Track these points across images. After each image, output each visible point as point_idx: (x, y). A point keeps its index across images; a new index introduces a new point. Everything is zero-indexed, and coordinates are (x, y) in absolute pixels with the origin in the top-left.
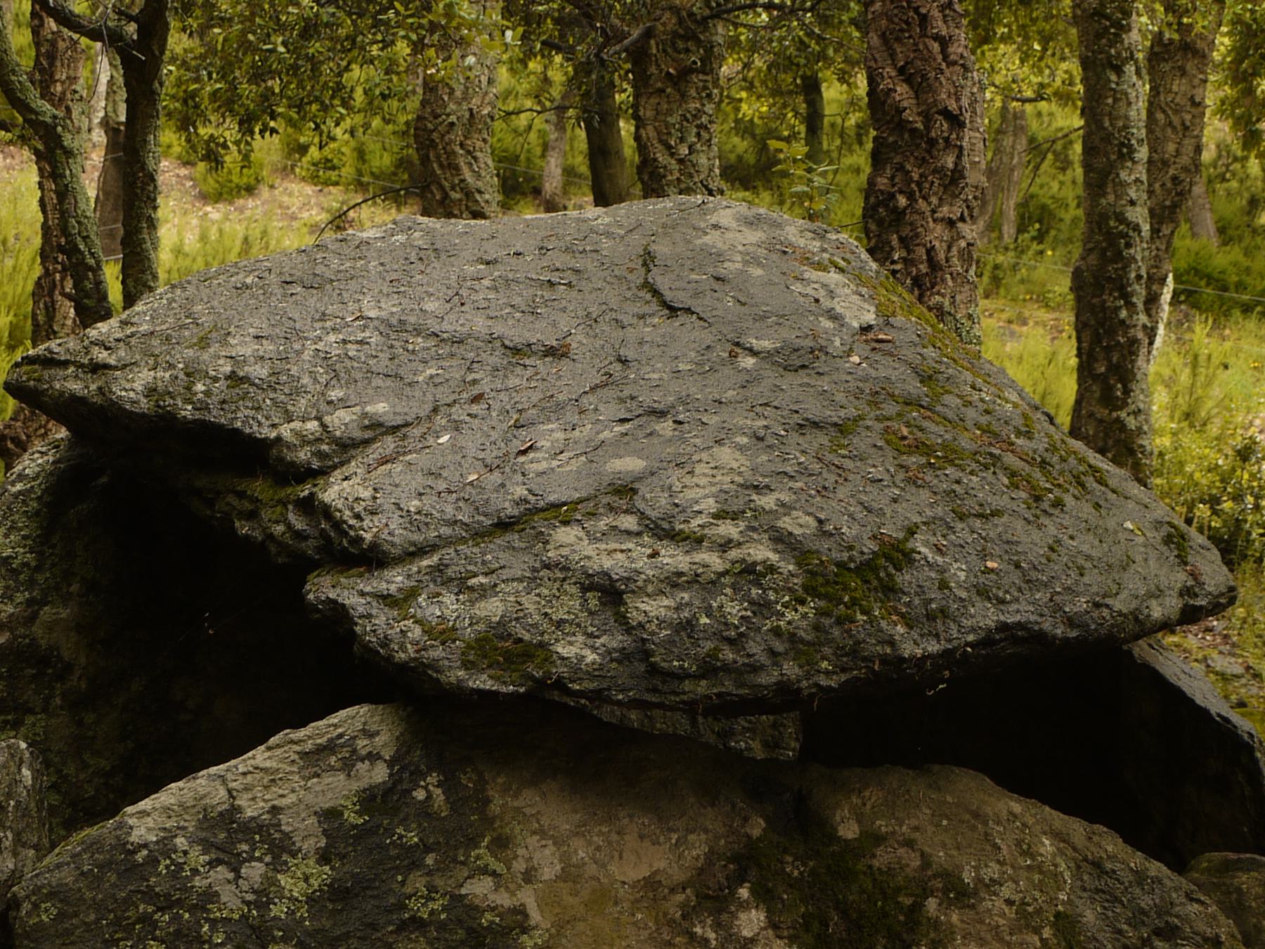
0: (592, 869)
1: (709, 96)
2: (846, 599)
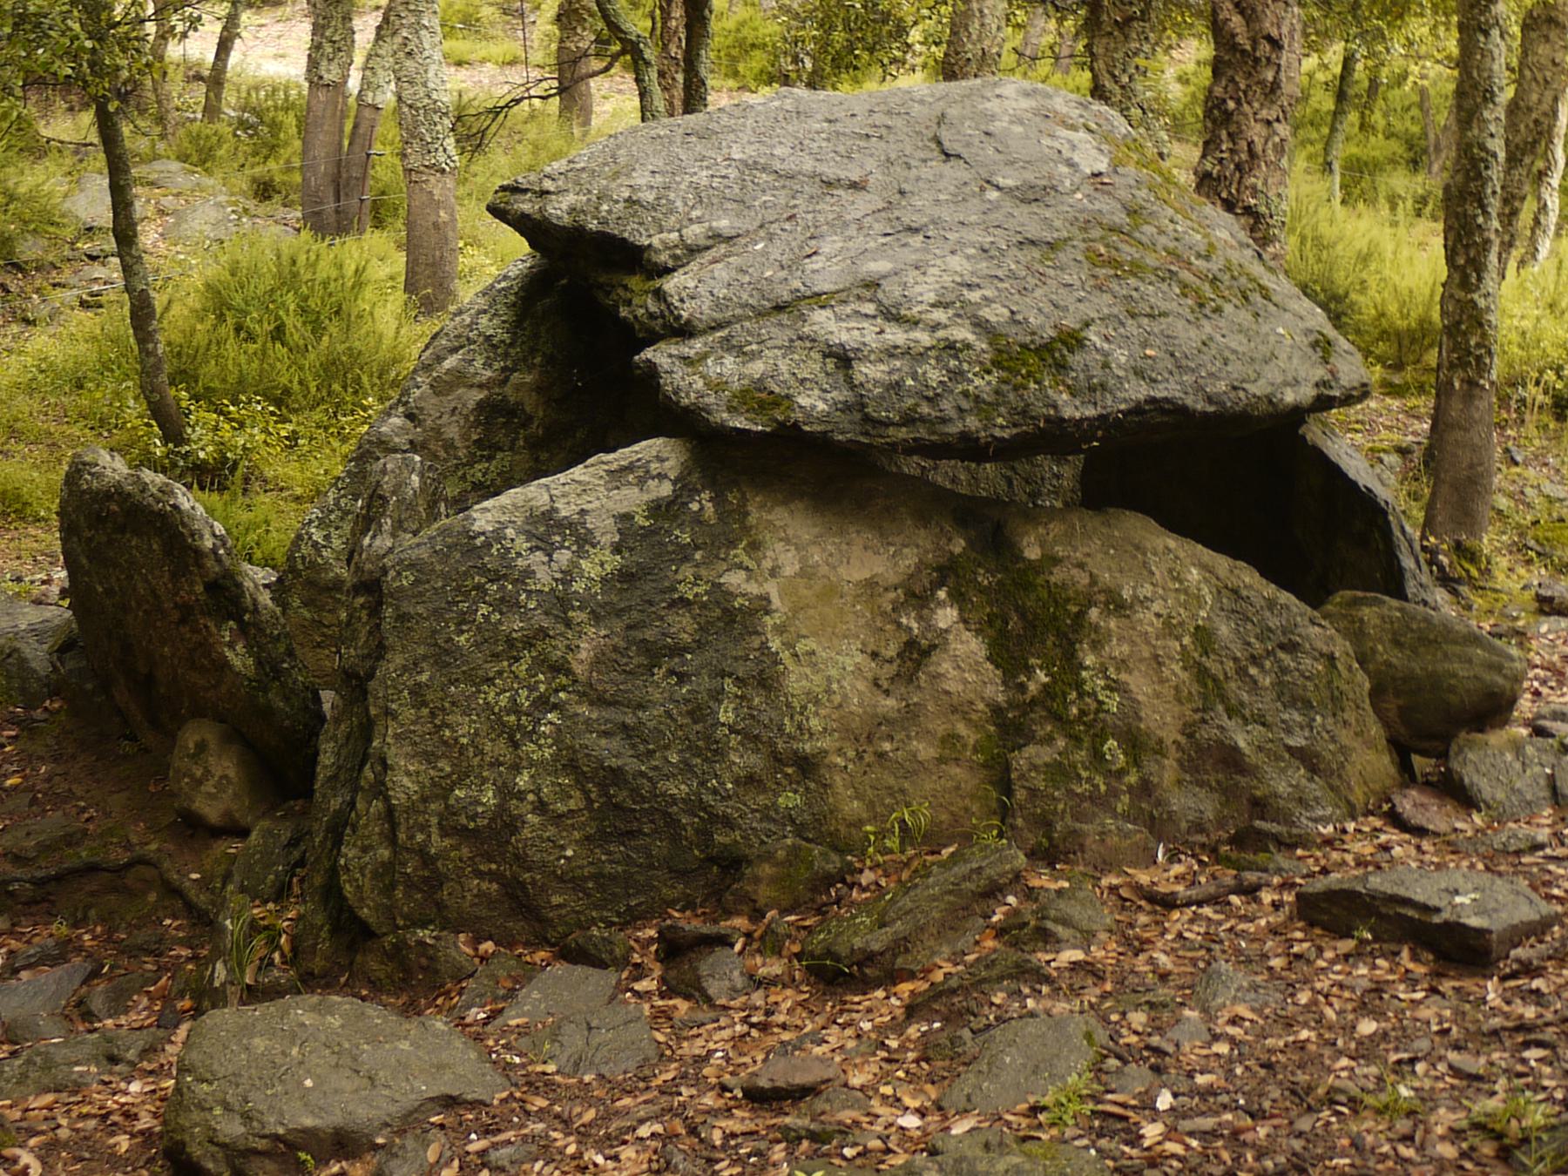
0: (824, 570)
1: (1147, 38)
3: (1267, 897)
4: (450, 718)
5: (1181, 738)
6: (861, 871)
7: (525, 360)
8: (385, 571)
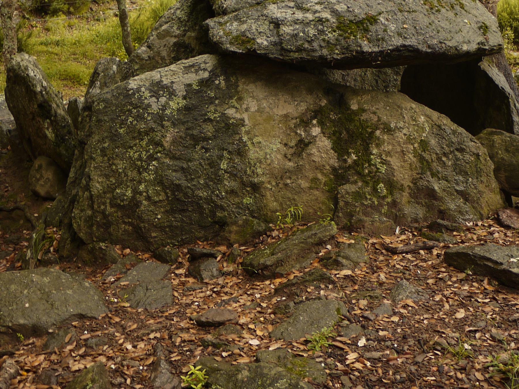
0: (268, 109)
2: (349, 31)
3: (435, 252)
4: (115, 162)
5: (410, 184)
6: (273, 230)
7: (192, 27)
8: (93, 102)
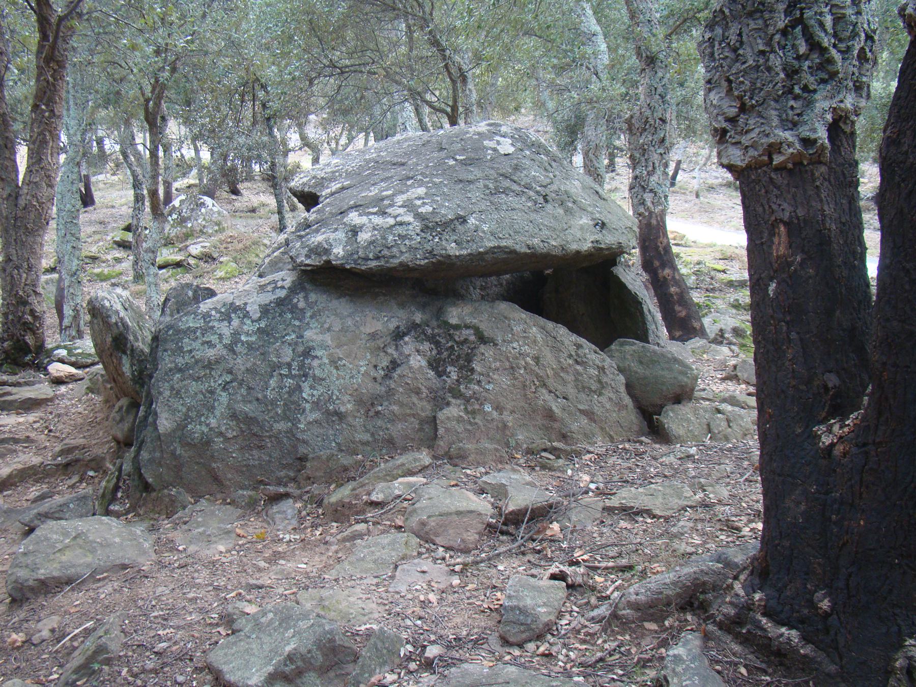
0: (353, 328)
